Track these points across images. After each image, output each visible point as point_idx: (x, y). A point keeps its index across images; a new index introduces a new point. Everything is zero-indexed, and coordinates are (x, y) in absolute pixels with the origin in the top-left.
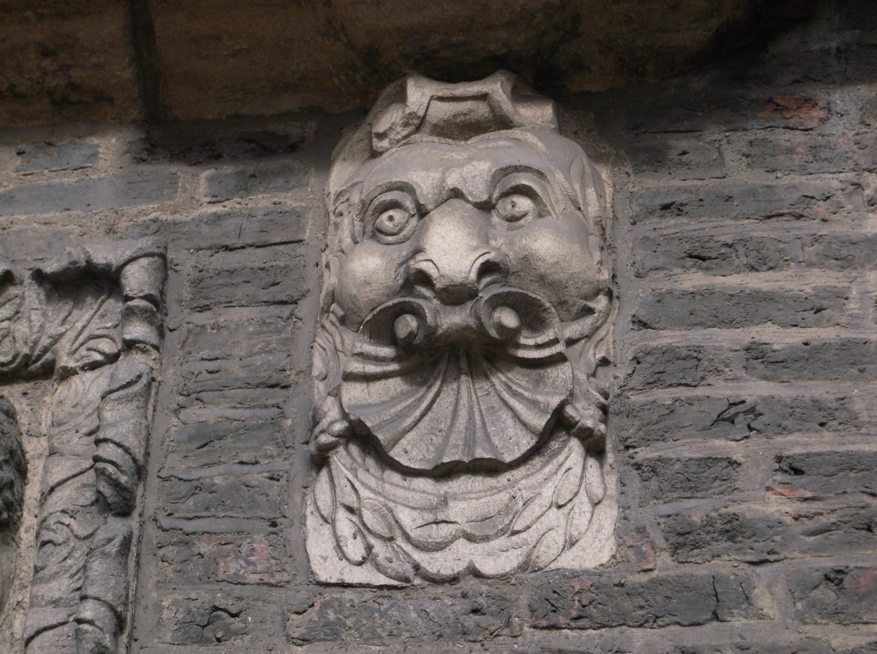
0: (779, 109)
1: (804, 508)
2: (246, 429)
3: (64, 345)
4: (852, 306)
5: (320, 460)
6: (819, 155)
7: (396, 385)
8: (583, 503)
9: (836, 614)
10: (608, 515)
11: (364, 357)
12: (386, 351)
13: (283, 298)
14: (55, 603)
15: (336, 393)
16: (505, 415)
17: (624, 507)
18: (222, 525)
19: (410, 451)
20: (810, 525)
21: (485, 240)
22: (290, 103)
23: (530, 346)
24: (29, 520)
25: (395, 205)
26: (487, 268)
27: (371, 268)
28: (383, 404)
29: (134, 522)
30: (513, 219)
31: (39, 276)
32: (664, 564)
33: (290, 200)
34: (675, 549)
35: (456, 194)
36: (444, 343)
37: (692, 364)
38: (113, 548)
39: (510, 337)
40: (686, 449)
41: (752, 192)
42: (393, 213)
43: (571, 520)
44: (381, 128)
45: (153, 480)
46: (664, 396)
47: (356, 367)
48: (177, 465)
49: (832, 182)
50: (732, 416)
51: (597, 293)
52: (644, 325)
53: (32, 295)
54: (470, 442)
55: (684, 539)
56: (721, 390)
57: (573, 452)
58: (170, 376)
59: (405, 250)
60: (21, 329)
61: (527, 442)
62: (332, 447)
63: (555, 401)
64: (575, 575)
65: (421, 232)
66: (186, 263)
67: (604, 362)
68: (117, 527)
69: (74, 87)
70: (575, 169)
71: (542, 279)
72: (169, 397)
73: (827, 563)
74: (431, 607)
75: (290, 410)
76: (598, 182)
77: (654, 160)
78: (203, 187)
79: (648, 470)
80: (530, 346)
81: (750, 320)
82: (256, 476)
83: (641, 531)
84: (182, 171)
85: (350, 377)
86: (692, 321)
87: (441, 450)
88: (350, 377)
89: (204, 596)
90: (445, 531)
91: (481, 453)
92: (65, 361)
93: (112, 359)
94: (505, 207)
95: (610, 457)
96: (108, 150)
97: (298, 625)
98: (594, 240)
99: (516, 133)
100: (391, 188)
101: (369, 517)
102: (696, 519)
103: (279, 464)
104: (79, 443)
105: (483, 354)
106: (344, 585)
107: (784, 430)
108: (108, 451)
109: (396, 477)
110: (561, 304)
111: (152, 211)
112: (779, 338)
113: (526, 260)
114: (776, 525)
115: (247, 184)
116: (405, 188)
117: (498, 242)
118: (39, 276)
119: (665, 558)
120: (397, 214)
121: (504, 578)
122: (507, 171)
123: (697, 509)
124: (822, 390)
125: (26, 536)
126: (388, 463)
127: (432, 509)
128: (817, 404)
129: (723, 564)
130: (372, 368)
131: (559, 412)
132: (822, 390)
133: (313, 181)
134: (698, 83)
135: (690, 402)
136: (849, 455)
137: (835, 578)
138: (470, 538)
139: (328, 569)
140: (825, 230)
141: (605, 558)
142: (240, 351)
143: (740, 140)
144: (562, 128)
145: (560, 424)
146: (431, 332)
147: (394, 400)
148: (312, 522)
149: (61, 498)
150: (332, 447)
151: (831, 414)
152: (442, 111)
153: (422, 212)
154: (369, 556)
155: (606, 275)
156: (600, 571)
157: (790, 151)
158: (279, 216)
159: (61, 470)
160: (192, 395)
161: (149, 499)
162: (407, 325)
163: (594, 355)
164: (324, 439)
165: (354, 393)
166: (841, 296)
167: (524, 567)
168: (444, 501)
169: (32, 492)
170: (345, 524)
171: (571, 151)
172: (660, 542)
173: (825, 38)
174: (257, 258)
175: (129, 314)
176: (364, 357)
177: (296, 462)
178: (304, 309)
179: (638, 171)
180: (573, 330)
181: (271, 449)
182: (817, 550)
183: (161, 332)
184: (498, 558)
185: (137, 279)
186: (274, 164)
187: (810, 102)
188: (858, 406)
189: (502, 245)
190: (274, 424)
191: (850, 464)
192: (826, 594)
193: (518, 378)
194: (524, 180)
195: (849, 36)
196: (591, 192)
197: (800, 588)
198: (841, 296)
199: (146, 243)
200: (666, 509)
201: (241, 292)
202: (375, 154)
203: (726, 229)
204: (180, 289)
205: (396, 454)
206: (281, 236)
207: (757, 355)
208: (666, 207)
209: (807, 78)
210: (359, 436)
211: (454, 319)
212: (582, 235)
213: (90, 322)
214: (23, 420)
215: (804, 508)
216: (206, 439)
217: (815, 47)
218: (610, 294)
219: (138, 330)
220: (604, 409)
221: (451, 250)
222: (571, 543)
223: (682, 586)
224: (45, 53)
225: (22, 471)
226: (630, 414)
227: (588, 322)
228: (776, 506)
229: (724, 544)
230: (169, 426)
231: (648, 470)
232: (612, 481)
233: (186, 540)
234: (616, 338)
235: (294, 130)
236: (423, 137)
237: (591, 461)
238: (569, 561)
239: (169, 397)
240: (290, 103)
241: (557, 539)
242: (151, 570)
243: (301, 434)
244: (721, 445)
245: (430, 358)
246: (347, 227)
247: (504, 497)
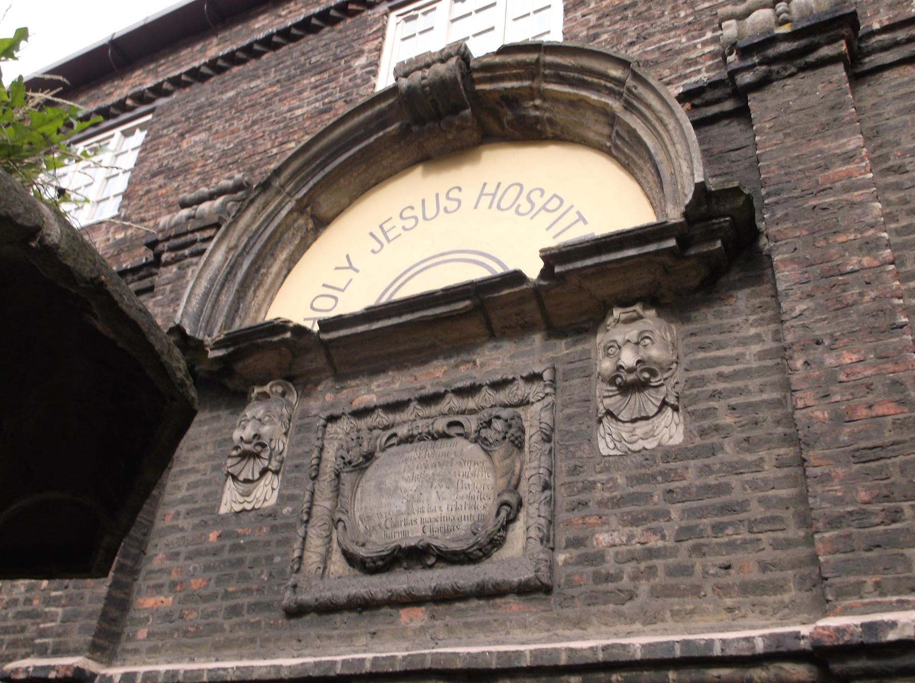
0: (722, 300)
1: (737, 420)
2: (580, 414)
3: (531, 396)
4: (747, 357)
5: (600, 421)
6: (736, 312)
7: (618, 397)
8: (673, 425)
9: (748, 451)
10: (681, 428)
11: (608, 391)
12: (614, 388)
13: (587, 374)
14: (535, 468)
15: (602, 402)
16: (649, 403)
17: (685, 425)
18: (576, 442)
19: (624, 416)
20: (739, 424)
21: (637, 353)
22: (585, 318)
23: (654, 382)
24: (527, 445)
25: (612, 346)
26: (638, 362)
27: (606, 365)
28: (615, 403)
29: (552, 444)
30: (645, 346)
31: (522, 377)
32: (698, 441)
33: (587, 346)
34: (701, 436)
35: (629, 341)
36: (630, 385)
37: (702, 381)
38: (547, 452)
39: (648, 381)
40: (702, 406)
41: (716, 327)
42: (613, 349)
43: (670, 430)
44: (608, 323)
45: (556, 431)
46: (695, 391)
47: (606, 394)
48: (563, 427)
49: (739, 320)
50: (714, 395)
51: (672, 363)
52: (688, 370)
53: (521, 383)
54: (640, 411)
55: (703, 433)
56: (711, 387)
57: (669, 411)
58: (559, 401)
59: (616, 359)
60: (519, 392)
61: (656, 410)
62: (602, 417)
63: (662, 397)
64: (673, 446)
65: (619, 354)
66: (560, 368)
67: (677, 383)
68: (547, 446)
69: (526, 323)
70: (663, 328)
71: (655, 363)
72: (559, 407)
73: (745, 435)
74: (634, 460)
75: (591, 407)
76: (670, 330)
77: (687, 320)
78: (563, 346)
79: (692, 413)
80: (654, 382)
81: (719, 364)
82: (584, 427)
83: (691, 431)
84: (557, 342)
85: (605, 397)
86: (701, 367)
87: (632, 415)
88: (605, 397)
89: (572, 463)
90: (635, 438)
91: (643, 414)
92: (532, 400)
93: (543, 398)
94: (642, 343)
95: (681, 411)
96: (537, 338)
97: (598, 468)
98: (670, 348)
99: (644, 320)
100: (611, 341)
101: (614, 436)
102: (706, 426)
103: (590, 423)
104: (537, 423)
105: (640, 386)
106: (609, 456)
107: (729, 397)
108: (543, 426)
109: (621, 424)
110: (662, 368)
111: (551, 354)
112: (726, 369)
113: (650, 358)
114: (729, 426)
115: (575, 343)
116: (615, 341)
117: (641, 353)
118: (522, 377)
119: (698, 439)
120: (613, 349)
121: (653, 449)
122: (642, 333)
123: (706, 423)
124: (739, 384)
125: (526, 449)
126: (618, 420)
127: (631, 432)
128: (739, 388)
129: (715, 439)
130: (611, 394)
131: (664, 399)
132: (739, 384)
133: (592, 340)
134: (698, 295)
135: (702, 392)
136: (749, 403)
137: (747, 440)
138: (642, 439)
139: (605, 451)
140: (738, 335)
141: (681, 440)
142: (577, 392)
143: (712, 311)
144: (659, 316)
145: (664, 403)
146: (625, 382)
147: (618, 402)
148: (599, 438)
149: (534, 438)
150: (602, 417)
151: (743, 390)
152: (623, 317)
153: (620, 348)
154: (615, 447)
155: (675, 358)
156: (680, 445)
157: (727, 312)
158: (585, 351)
159: (532, 432)
160: (565, 406)
161: (556, 437)
162: (619, 380)
163: (673, 381)
164: (600, 415)
165: (607, 401)
166: (743, 355)
167: (659, 445)
168: (634, 429)
169: (527, 437)
170: (608, 438)
171: (662, 323)
172: (696, 434)
173: (734, 276)
174: (579, 364)
175: (545, 386)
176: (608, 391)
177: (594, 422)
178: (593, 378)
179: (683, 324)
180: (665, 376)
181: (587, 419)
182: (742, 432)
183: (555, 389)
184: (651, 444)
185: (547, 375)
186: (581, 337)
187: (731, 296)
188: (751, 387)
189: (643, 354)
190: (587, 412)
191: (749, 405)
192: (745, 445)
193: (652, 391)
194: (647, 334)
195: (741, 274)
196: (668, 334)
197: (738, 443)
198: (743, 355)
199: (548, 365)
200: (697, 424)
201: (576, 375)
202: (608, 331)
203: (708, 338)
204: (559, 376)
205: (620, 417)
206: (586, 357)
207: (721, 376)
208: (692, 334)
209: (730, 289)
210: (609, 413)
211: (631, 377)
212: (666, 347)
213: (534, 391)
214: (523, 417)
215: (737, 420)
216: (569, 418)
217: (731, 279)
218: (677, 363)
219: (548, 390)
220: (678, 398)
221: (628, 358)
222: (671, 437)
223: (703, 447)
224: (517, 315)
225: (524, 432)
226: (685, 397)
227: (671, 372)
228: (729, 420)
229: (715, 433)
230: (560, 416)
231: (692, 413)
232: (681, 418)
233: (567, 447)
234: (680, 375)
235: (586, 326)
236: (620, 325)
237: (675, 413)
238: (671, 442)
239: (559, 407)
240: (585, 318)
241: (667, 436)
242: (558, 456)
243: (595, 414)
244: (712, 404)
245: (627, 389)
246: (601, 354)
247: (651, 426)
